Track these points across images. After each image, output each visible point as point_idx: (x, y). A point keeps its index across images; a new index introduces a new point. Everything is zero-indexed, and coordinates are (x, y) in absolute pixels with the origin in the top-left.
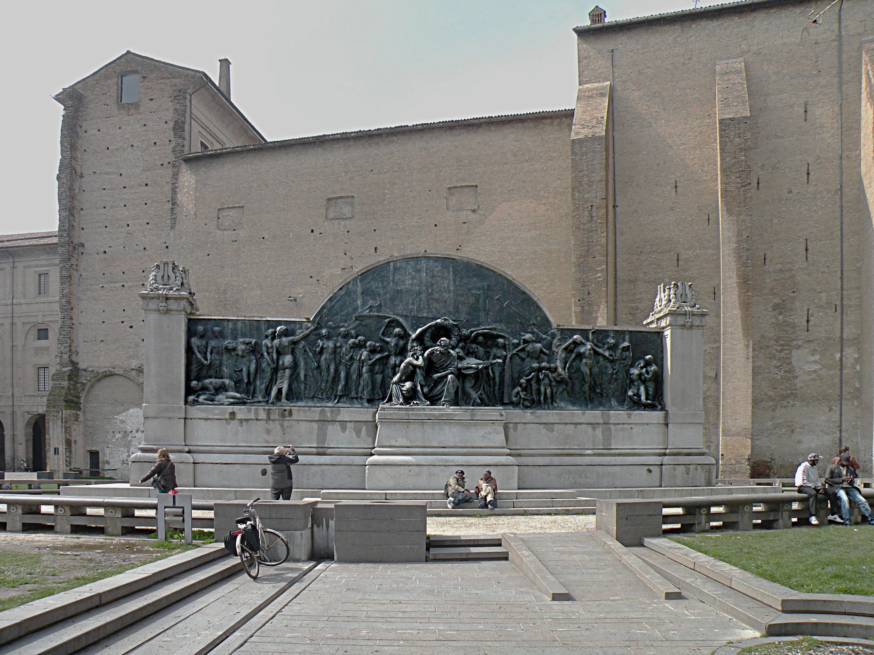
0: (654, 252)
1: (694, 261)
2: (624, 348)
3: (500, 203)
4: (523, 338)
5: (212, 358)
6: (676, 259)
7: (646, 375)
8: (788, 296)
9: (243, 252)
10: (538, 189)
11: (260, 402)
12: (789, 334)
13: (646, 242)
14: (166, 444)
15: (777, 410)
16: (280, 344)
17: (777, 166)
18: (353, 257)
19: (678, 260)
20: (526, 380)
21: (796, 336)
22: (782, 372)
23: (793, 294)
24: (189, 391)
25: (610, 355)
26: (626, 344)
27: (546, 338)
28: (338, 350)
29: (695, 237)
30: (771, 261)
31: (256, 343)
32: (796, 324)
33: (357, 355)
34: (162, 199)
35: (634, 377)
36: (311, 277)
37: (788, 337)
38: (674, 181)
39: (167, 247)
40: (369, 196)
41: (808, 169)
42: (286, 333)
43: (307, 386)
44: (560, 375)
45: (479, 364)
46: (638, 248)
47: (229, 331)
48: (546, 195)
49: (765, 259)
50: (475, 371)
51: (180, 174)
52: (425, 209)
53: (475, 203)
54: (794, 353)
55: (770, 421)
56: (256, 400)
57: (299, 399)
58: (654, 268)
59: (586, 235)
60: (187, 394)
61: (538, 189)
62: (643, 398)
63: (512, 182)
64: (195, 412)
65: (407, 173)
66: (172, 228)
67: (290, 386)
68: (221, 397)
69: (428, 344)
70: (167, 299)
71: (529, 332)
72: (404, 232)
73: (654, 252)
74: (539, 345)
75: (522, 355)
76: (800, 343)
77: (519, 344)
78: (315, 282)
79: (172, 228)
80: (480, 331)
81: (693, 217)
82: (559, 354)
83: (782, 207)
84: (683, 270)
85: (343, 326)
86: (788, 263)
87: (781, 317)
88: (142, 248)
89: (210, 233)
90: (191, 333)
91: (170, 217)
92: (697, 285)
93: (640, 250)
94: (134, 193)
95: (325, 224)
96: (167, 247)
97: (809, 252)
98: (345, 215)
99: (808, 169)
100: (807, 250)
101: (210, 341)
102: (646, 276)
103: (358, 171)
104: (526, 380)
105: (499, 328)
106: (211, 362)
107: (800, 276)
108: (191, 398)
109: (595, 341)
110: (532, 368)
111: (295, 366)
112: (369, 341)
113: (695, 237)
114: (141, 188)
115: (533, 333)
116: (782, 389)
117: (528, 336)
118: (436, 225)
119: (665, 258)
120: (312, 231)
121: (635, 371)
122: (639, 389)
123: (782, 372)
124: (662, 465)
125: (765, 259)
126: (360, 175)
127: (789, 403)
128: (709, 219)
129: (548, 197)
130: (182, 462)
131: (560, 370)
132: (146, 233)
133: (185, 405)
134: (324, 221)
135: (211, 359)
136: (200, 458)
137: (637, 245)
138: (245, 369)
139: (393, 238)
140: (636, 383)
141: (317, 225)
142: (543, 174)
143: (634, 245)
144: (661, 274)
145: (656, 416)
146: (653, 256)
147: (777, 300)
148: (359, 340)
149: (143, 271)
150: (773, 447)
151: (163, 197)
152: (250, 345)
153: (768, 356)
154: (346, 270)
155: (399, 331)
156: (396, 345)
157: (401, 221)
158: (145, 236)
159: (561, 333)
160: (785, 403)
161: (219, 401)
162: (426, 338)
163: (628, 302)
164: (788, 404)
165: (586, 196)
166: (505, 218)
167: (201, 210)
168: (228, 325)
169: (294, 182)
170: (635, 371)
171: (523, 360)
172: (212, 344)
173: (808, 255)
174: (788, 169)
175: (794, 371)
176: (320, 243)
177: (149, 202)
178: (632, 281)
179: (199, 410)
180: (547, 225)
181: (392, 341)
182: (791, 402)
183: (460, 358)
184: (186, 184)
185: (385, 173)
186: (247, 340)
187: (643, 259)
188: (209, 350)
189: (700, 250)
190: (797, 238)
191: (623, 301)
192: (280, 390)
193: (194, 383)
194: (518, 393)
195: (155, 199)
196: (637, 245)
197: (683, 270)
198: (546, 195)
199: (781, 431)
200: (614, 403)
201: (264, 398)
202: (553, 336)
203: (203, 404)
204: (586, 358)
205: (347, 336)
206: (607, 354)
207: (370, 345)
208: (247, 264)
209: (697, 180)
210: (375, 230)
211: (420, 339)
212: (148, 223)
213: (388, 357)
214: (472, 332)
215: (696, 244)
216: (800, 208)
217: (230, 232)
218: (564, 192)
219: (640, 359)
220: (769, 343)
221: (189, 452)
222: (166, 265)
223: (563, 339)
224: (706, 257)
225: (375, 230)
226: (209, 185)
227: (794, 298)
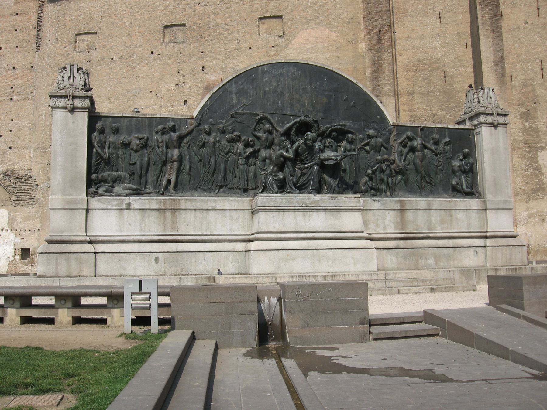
0: (426, 69)
1: (457, 77)
2: (445, 143)
3: (300, 31)
4: (368, 133)
5: (110, 152)
6: (444, 75)
7: (465, 167)
8: (531, 106)
9: (96, 70)
10: (329, 19)
11: (151, 193)
12: (535, 138)
13: (419, 61)
14: (70, 235)
15: (530, 202)
16: (169, 139)
17: (515, 2)
18: (185, 74)
19: (445, 77)
20: (372, 170)
21: (539, 140)
22: (532, 170)
23: (535, 105)
24: (90, 183)
25: (436, 149)
26: (447, 139)
27: (385, 134)
28: (218, 145)
29: (457, 58)
30: (516, 77)
31: (148, 138)
32: (540, 129)
33: (234, 149)
34: (29, 26)
35: (456, 169)
36: (151, 91)
37: (534, 140)
38: (438, 12)
39: (32, 67)
40: (197, 24)
41: (538, 5)
42: (173, 129)
43: (192, 178)
44: (398, 166)
45: (337, 156)
46: (413, 66)
47: (125, 127)
48: (336, 24)
49: (511, 76)
50: (335, 162)
51: (45, 6)
52: (241, 35)
53: (280, 31)
54: (539, 154)
55: (526, 211)
56: (148, 190)
57: (184, 190)
58: (427, 83)
59: (377, 55)
60: (89, 186)
61: (329, 19)
62: (464, 186)
63: (309, 13)
64: (95, 203)
65: (227, 5)
66: (37, 50)
67: (177, 177)
68: (117, 189)
69: (294, 138)
70: (74, 97)
71: (371, 129)
72: (225, 54)
73: (426, 69)
74: (380, 140)
75: (367, 148)
76: (543, 145)
77: (364, 139)
78: (154, 96)
79: (37, 50)
80: (334, 127)
81: (454, 41)
82: (396, 148)
83: (521, 34)
84: (450, 84)
85: (221, 123)
86: (529, 80)
87: (527, 124)
88: (12, 68)
89: (68, 54)
90: (91, 129)
91: (35, 41)
92: (461, 97)
93: (415, 68)
94: (6, 22)
95: (163, 47)
96: (32, 67)
97: (544, 70)
98: (178, 40)
99: (538, 5)
100: (542, 69)
101: (108, 137)
102: (421, 90)
103: (188, 4)
104: (372, 170)
105: (349, 124)
106: (109, 156)
107: (539, 90)
108: (92, 190)
109: (423, 136)
110: (376, 160)
111: (180, 160)
112: (244, 136)
113: (457, 58)
114: (12, 17)
115: (375, 129)
116: (532, 184)
117: (371, 132)
118: (250, 48)
119: (435, 74)
120: (152, 53)
121: (456, 163)
122: (460, 179)
123: (532, 170)
124: (485, 247)
125: (511, 76)
126: (190, 7)
127: (539, 195)
128: (466, 44)
129: (338, 26)
130: (85, 253)
131: (398, 162)
132: (15, 55)
133: (87, 196)
134: (161, 44)
135: (109, 153)
136: (100, 247)
137: (412, 64)
138: (138, 162)
139: (217, 59)
140: (458, 174)
141: (156, 48)
142: (333, 8)
143: (410, 64)
144: (433, 88)
145: (474, 203)
146: (426, 73)
147: (523, 110)
148: (235, 135)
149: (12, 88)
150: (530, 233)
151: (31, 25)
152: (143, 140)
153: (520, 156)
154: (180, 85)
155: (269, 127)
156: (267, 139)
157: (223, 45)
158: (14, 58)
159: (397, 130)
160: (536, 195)
161: (116, 193)
162: (292, 133)
163: (408, 111)
164: (538, 197)
165: (375, 23)
166: (305, 42)
167: (62, 36)
168: (124, 122)
169: (137, 12)
170: (456, 163)
171: (368, 152)
172: (111, 139)
173: (544, 73)
174: (523, 5)
175: (541, 168)
176: (158, 63)
177: (18, 29)
178: (410, 93)
179: (99, 201)
180: (337, 48)
181: (262, 135)
182: (541, 195)
183: (322, 151)
184: (50, 14)
185: (210, 5)
186: (140, 136)
187: (417, 75)
188: (107, 145)
189: (461, 68)
190: (534, 60)
191: (404, 110)
192: (169, 181)
193: (94, 176)
194: (366, 183)
195: (23, 26)
196: (412, 64)
197: (450, 84)
198: (336, 24)
199: (535, 220)
200: (440, 189)
201: (155, 189)
202: (391, 132)
203: (102, 195)
204: (418, 151)
205: (223, 132)
206: (433, 148)
207: (245, 140)
208: (99, 80)
209: (455, 12)
210: (202, 52)
211: (287, 134)
212: (17, 47)
213: (258, 151)
214: (328, 128)
215: (458, 63)
216: (534, 35)
217: (85, 54)
218: (350, 22)
219: (458, 152)
220: (519, 145)
221: (90, 242)
222: (72, 67)
223: (398, 135)
224: (466, 74)
225: (202, 52)
226: (69, 14)
227: (535, 109)
